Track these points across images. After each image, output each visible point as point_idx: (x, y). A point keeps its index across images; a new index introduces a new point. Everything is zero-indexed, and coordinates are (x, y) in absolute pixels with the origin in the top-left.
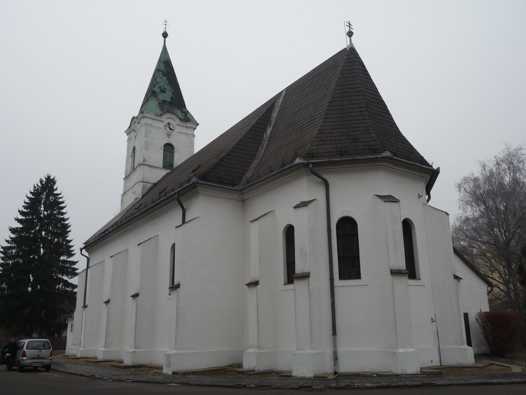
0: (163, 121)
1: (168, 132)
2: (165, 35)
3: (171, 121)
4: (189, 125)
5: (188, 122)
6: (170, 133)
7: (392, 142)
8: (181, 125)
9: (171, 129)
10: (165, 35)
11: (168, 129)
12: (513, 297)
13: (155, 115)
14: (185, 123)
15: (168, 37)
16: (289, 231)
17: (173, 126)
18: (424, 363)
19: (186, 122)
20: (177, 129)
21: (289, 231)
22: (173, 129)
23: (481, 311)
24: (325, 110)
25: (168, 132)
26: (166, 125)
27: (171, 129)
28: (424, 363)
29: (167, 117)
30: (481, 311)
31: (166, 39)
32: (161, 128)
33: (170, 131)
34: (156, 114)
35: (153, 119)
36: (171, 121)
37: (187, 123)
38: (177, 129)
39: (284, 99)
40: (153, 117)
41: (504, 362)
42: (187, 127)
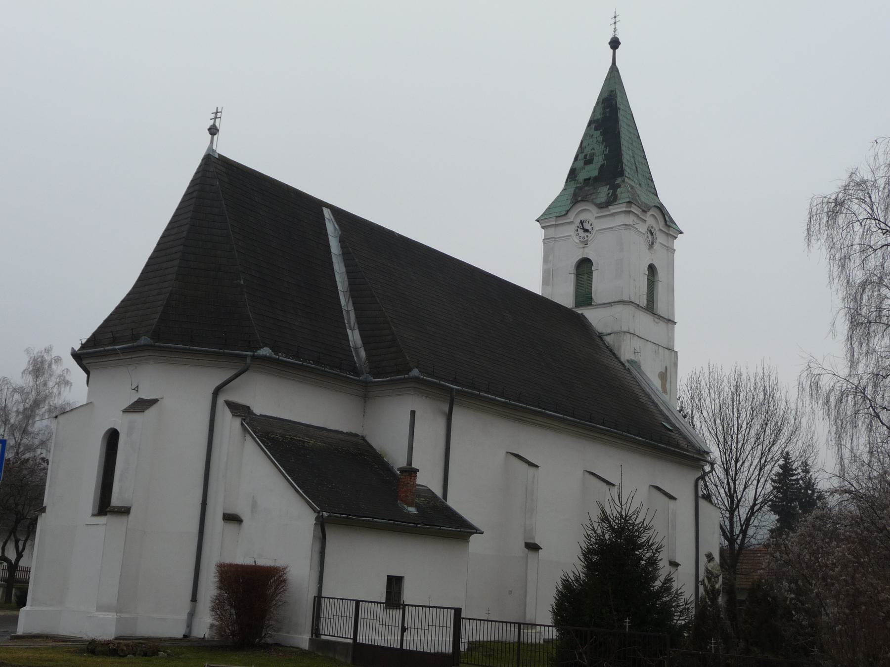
0: (572, 222)
1: (582, 237)
2: (615, 44)
3: (583, 217)
4: (614, 209)
5: (610, 205)
6: (586, 239)
7: (627, 124)
8: (602, 216)
9: (586, 231)
10: (615, 44)
11: (581, 232)
12: (739, 543)
13: (557, 217)
14: (607, 209)
15: (620, 46)
16: (112, 438)
17: (590, 223)
18: (81, 632)
19: (607, 207)
20: (598, 225)
21: (112, 438)
22: (590, 230)
23: (255, 562)
24: (187, 224)
25: (582, 237)
26: (578, 227)
27: (586, 231)
28: (81, 632)
29: (576, 215)
30: (255, 562)
31: (616, 50)
32: (570, 236)
33: (585, 234)
34: (558, 215)
35: (556, 225)
36: (583, 217)
37: (610, 207)
38: (598, 225)
39: (169, 235)
40: (554, 223)
41: (16, 642)
42: (613, 214)
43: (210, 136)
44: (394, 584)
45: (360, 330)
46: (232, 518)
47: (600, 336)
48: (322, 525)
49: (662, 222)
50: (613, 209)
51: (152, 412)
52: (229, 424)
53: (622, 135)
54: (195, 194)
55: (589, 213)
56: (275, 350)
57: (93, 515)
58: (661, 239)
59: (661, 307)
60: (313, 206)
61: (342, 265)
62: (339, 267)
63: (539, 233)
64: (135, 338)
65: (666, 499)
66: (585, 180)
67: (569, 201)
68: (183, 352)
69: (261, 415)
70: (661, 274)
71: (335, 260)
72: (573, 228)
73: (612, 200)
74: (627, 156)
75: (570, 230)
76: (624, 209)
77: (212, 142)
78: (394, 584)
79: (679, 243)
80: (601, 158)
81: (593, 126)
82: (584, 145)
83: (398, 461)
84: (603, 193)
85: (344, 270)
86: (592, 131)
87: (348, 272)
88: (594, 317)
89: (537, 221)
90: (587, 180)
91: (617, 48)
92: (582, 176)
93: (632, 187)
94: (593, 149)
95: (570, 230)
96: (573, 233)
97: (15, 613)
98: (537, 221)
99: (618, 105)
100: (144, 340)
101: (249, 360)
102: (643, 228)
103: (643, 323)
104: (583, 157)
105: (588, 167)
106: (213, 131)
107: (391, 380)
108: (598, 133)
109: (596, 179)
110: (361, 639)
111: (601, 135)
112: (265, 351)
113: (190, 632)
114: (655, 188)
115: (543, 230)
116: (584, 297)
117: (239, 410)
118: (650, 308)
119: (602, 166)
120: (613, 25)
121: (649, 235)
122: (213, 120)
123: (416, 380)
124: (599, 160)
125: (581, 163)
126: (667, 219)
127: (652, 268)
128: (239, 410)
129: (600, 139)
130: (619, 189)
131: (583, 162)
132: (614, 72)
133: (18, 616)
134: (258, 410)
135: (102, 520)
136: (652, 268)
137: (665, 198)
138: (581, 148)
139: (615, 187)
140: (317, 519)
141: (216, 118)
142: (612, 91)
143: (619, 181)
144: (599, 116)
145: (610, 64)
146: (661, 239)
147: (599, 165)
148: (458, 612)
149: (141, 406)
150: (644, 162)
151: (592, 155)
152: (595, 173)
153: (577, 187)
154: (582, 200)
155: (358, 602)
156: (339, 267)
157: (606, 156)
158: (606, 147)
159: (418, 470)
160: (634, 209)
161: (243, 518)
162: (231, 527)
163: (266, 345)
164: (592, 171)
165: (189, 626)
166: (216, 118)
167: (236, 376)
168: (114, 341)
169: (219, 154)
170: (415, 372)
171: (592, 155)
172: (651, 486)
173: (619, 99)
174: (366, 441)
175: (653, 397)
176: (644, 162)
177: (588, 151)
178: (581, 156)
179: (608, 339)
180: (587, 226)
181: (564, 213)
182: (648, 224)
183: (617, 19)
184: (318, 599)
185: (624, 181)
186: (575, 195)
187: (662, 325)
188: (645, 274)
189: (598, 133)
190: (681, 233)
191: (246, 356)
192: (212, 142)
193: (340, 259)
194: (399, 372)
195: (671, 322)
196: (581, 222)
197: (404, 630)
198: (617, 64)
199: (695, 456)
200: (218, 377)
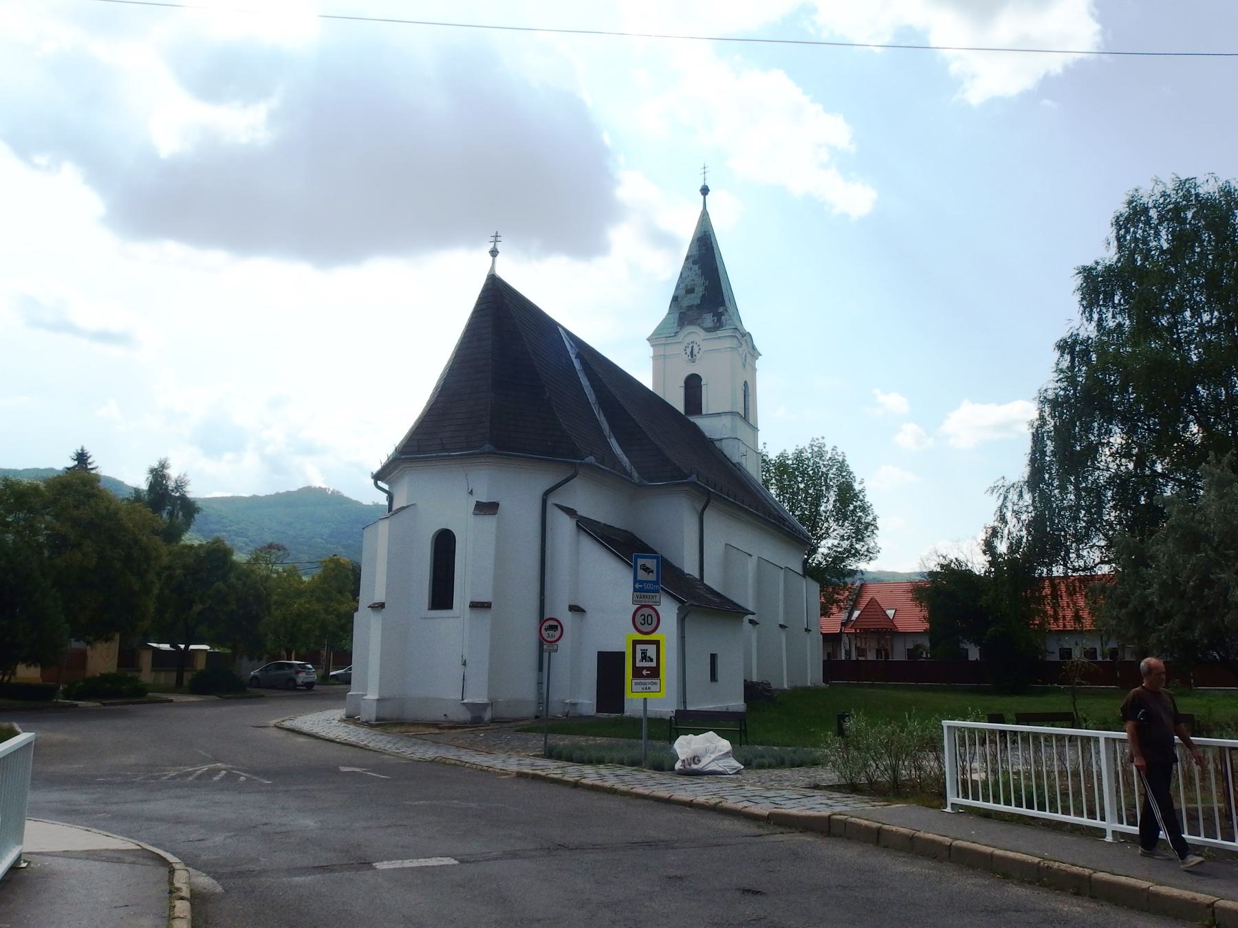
2: (705, 191)
3: (690, 339)
10: (705, 191)
20: (705, 346)
34: (668, 336)
35: (665, 344)
37: (718, 332)
43: (491, 258)
50: (720, 333)
52: (563, 527)
55: (695, 335)
68: (506, 455)
76: (730, 334)
81: (691, 261)
91: (707, 194)
92: (686, 302)
105: (690, 296)
108: (696, 267)
109: (699, 307)
111: (699, 269)
118: (745, 418)
119: (704, 295)
120: (703, 175)
122: (493, 243)
124: (700, 291)
125: (683, 292)
129: (699, 272)
130: (723, 317)
132: (705, 217)
136: (746, 384)
137: (748, 326)
144: (695, 252)
147: (700, 294)
156: (585, 382)
157: (706, 287)
164: (695, 299)
166: (496, 241)
167: (566, 481)
170: (694, 478)
179: (717, 444)
183: (706, 170)
187: (749, 430)
189: (696, 267)
190: (761, 355)
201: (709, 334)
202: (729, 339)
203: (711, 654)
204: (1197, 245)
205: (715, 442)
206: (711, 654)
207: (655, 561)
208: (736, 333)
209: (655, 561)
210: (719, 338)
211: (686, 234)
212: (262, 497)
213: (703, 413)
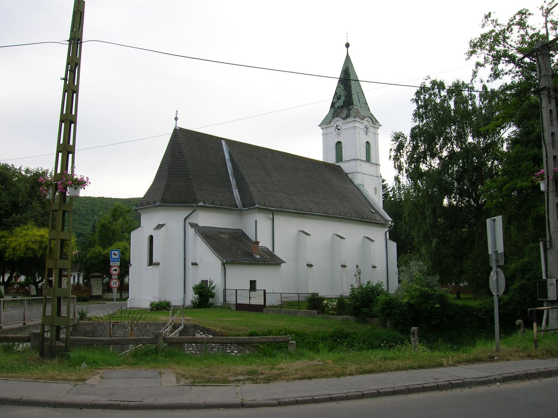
2: (347, 45)
9: (339, 129)
10: (347, 45)
11: (337, 130)
16: (151, 238)
19: (346, 119)
20: (343, 127)
21: (151, 238)
34: (327, 123)
35: (327, 128)
38: (343, 127)
44: (253, 284)
45: (238, 189)
46: (194, 264)
47: (347, 174)
48: (224, 264)
49: (371, 122)
50: (348, 120)
51: (163, 229)
52: (191, 231)
53: (352, 87)
54: (170, 151)
55: (339, 121)
56: (204, 203)
57: (148, 266)
58: (371, 130)
59: (373, 159)
60: (217, 141)
61: (230, 163)
62: (229, 165)
63: (321, 131)
64: (155, 203)
65: (369, 241)
66: (338, 107)
67: (332, 117)
69: (202, 226)
70: (372, 145)
71: (227, 162)
72: (334, 128)
73: (348, 116)
74: (354, 97)
75: (332, 130)
76: (353, 120)
77: (176, 124)
78: (253, 284)
79: (380, 131)
80: (344, 97)
81: (340, 83)
82: (337, 92)
83: (253, 238)
84: (345, 112)
85: (231, 165)
86: (340, 85)
87: (232, 166)
88: (345, 167)
89: (319, 126)
90: (338, 107)
92: (337, 105)
93: (357, 109)
94: (340, 93)
95: (332, 130)
96: (334, 131)
97: (125, 302)
98: (319, 126)
99: (350, 73)
100: (158, 204)
101: (195, 207)
102: (362, 127)
103: (365, 167)
104: (337, 96)
105: (339, 101)
106: (176, 119)
107: (249, 209)
109: (342, 107)
110: (238, 302)
111: (343, 87)
112: (201, 204)
113: (184, 304)
114: (368, 108)
115: (322, 130)
116: (339, 157)
117: (193, 225)
118: (368, 160)
119: (344, 100)
121: (366, 129)
123: (258, 208)
124: (343, 98)
125: (336, 100)
126: (374, 120)
127: (368, 143)
128: (194, 226)
129: (343, 88)
131: (336, 99)
133: (127, 303)
134: (200, 225)
135: (151, 267)
136: (368, 143)
137: (373, 110)
138: (336, 93)
139: (349, 110)
140: (222, 263)
141: (177, 114)
142: (347, 67)
143: (351, 107)
145: (346, 55)
146: (371, 130)
148: (265, 291)
149: (160, 227)
150: (363, 96)
151: (340, 96)
152: (342, 104)
153: (334, 110)
154: (336, 116)
155: (236, 290)
156: (229, 165)
158: (345, 92)
159: (198, 265)
160: (357, 119)
161: (198, 264)
162: (195, 267)
163: (201, 201)
164: (340, 103)
165: (184, 302)
166: (177, 114)
167: (192, 213)
168: (148, 204)
169: (179, 128)
170: (257, 205)
171: (340, 96)
172: (366, 237)
173: (350, 70)
174: (243, 231)
175: (368, 199)
176: (363, 96)
177: (338, 94)
178: (336, 96)
179: (350, 176)
180: (339, 128)
181: (329, 122)
182: (365, 124)
184: (225, 290)
185: (353, 107)
186: (334, 114)
187: (374, 167)
188: (364, 146)
191: (194, 206)
192: (176, 124)
193: (230, 161)
194: (251, 205)
195: (378, 165)
196: (337, 126)
197: (250, 298)
198: (349, 54)
199: (383, 223)
200: (186, 213)
201: (344, 120)
202: (352, 123)
203: (251, 281)
204: (474, 180)
205: (348, 175)
206: (251, 281)
207: (118, 252)
208: (356, 119)
209: (118, 252)
210: (349, 122)
211: (338, 73)
212: (143, 198)
213: (343, 160)
